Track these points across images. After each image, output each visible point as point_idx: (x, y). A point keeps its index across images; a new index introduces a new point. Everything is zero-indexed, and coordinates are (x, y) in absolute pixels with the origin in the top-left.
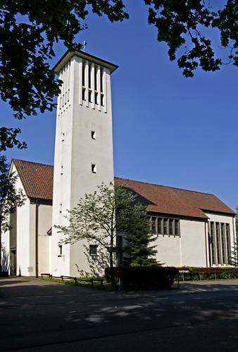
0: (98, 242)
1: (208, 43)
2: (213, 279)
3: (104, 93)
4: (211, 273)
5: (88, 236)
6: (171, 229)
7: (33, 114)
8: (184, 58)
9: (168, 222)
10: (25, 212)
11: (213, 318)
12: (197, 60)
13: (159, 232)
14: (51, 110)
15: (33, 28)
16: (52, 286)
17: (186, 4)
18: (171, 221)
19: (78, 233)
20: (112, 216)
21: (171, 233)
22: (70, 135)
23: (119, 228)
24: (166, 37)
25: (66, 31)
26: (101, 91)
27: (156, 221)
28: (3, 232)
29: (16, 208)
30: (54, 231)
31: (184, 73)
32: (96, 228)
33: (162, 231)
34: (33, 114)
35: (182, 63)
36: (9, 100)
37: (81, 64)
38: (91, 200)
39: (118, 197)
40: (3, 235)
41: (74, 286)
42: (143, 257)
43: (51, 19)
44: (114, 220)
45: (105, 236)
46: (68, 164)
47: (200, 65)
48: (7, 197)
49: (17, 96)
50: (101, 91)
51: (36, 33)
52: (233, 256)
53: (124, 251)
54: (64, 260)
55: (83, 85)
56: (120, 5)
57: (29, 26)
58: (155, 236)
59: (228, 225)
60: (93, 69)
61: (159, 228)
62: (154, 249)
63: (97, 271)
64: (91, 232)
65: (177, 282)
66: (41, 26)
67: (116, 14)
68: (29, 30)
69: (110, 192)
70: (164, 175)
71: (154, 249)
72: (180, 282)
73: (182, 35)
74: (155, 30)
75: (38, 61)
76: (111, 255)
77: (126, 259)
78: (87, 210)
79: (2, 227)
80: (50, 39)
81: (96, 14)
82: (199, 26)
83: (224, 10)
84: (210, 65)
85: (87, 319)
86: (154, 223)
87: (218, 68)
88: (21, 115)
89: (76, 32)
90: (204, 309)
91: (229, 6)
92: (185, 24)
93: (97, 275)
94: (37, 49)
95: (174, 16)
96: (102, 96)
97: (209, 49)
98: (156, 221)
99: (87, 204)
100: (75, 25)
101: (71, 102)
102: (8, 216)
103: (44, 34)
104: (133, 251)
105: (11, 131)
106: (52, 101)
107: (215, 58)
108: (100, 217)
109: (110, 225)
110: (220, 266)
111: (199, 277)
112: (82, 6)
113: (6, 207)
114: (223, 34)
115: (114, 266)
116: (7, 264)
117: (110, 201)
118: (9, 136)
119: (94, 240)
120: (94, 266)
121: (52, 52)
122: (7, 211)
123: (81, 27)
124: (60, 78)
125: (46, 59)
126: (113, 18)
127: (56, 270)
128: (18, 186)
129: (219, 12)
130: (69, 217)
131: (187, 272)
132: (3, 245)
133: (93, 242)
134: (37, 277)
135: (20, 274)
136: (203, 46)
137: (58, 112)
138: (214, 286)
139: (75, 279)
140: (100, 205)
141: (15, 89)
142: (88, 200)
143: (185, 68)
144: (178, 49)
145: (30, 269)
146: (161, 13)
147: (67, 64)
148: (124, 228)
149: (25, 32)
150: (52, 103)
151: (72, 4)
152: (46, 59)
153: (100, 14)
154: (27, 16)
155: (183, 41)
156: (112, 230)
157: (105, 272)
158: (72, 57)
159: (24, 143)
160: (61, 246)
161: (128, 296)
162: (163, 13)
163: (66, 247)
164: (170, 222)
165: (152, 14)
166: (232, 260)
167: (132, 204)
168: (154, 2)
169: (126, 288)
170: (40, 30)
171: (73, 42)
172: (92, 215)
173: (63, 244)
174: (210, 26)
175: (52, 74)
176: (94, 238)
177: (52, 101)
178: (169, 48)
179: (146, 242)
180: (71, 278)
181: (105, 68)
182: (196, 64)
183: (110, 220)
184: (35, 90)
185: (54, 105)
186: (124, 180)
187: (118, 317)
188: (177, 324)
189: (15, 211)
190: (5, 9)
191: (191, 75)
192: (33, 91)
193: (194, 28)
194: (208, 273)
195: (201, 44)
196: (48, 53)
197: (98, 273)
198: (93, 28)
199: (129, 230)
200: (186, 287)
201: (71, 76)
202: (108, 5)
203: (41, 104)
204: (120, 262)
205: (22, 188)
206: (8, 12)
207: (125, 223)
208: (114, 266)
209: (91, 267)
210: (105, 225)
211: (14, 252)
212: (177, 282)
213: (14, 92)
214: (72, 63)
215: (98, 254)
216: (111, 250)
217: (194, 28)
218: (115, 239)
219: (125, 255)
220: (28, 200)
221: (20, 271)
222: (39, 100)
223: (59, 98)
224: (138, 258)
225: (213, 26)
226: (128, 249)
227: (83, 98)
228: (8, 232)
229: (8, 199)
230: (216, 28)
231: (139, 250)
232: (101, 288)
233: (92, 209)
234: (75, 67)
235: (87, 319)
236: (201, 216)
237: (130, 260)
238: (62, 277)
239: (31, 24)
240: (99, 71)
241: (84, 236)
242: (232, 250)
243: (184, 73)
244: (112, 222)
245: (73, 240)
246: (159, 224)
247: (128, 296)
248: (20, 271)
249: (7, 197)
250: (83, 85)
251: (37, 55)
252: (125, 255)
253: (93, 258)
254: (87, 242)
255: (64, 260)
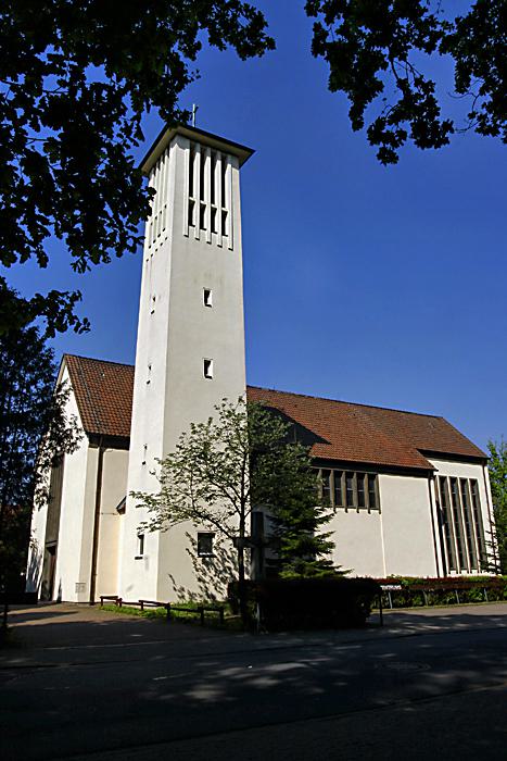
0: (214, 527)
1: (428, 87)
2: (453, 602)
3: (227, 208)
4: (448, 591)
5: (196, 514)
6: (361, 496)
7: (104, 261)
8: (380, 123)
9: (354, 481)
10: (79, 462)
11: (458, 687)
12: (406, 125)
13: (338, 503)
14: (133, 250)
15: (110, 89)
16: (120, 623)
17: (391, 8)
18: (360, 477)
19: (176, 509)
20: (243, 469)
21: (361, 505)
22: (166, 301)
23: (257, 495)
24: (346, 82)
25: (163, 89)
26: (223, 205)
27: (331, 477)
28: (36, 506)
29: (63, 455)
30: (131, 503)
31: (379, 156)
32: (210, 498)
33: (344, 501)
34: (104, 261)
35: (376, 135)
36: (66, 235)
37: (188, 151)
38: (203, 437)
39: (255, 429)
40: (35, 513)
41: (164, 624)
42: (307, 557)
43: (139, 68)
44: (246, 478)
45: (229, 514)
46: (160, 363)
47: (411, 137)
48: (49, 434)
49: (79, 226)
50: (223, 205)
51: (115, 98)
52: (489, 550)
53: (267, 545)
54: (147, 565)
55: (191, 194)
56: (258, 22)
57: (105, 87)
58: (329, 511)
59: (474, 482)
60: (208, 160)
61: (338, 494)
62: (327, 540)
63: (212, 590)
64: (202, 504)
65: (378, 611)
66: (123, 83)
67: (252, 42)
68: (104, 93)
69: (239, 418)
70: (349, 381)
71: (327, 540)
72: (385, 612)
73: (379, 75)
74: (323, 67)
75: (116, 153)
76: (241, 555)
77: (270, 561)
78: (195, 459)
79: (35, 497)
80: (137, 107)
81: (216, 47)
82: (414, 53)
83: (469, 17)
84: (431, 134)
85: (190, 694)
86: (327, 483)
87: (446, 141)
88: (85, 264)
89: (180, 88)
90: (438, 665)
91: (481, 8)
92: (386, 51)
93: (213, 597)
94: (116, 128)
95: (363, 35)
96: (224, 214)
97: (431, 101)
98: (331, 477)
99: (195, 445)
100: (179, 70)
101: (169, 231)
102: (47, 475)
103: (127, 100)
104: (286, 544)
105: (65, 298)
106: (136, 231)
107: (440, 119)
108: (217, 472)
109: (238, 489)
110: (464, 573)
111: (423, 601)
112: (192, 32)
113: (46, 455)
114: (460, 67)
115: (246, 577)
116: (36, 577)
117: (239, 437)
118: (62, 307)
119: (208, 522)
120: (207, 579)
121: (140, 134)
122: (47, 463)
123: (189, 76)
124: (150, 185)
125: (129, 147)
126: (245, 52)
127: (130, 588)
128: (71, 409)
129: (457, 20)
130: (159, 474)
131: (398, 587)
132: (34, 536)
133: (204, 526)
134: (92, 603)
135: (60, 598)
136: (418, 96)
137: (147, 253)
138: (455, 619)
139: (167, 606)
140: (219, 447)
141: (77, 212)
142: (196, 437)
143: (382, 145)
144: (368, 105)
145: (80, 586)
146: (338, 32)
147: (163, 154)
148: (265, 495)
149: (99, 97)
150: (137, 235)
151: (175, 33)
152: (129, 147)
153: (222, 47)
154: (103, 66)
155: (379, 86)
156: (243, 501)
157: (228, 589)
158: (172, 139)
159: (86, 320)
160: (141, 537)
161: (276, 643)
162: (342, 31)
163: (153, 538)
164: (357, 482)
165: (320, 33)
166: (490, 560)
167: (282, 442)
168: (325, 9)
169: (272, 625)
170: (122, 92)
171: (175, 109)
172: (203, 467)
173: (146, 532)
174: (435, 52)
175: (137, 181)
176: (207, 517)
177: (136, 231)
178: (351, 104)
179: (311, 524)
180: (159, 604)
181: (229, 158)
182: (403, 135)
183: (240, 479)
184: (107, 210)
185: (140, 241)
186: (265, 391)
187: (255, 690)
188: (383, 702)
189: (62, 462)
190: (72, 59)
191: (393, 158)
192: (105, 214)
193: (403, 58)
194: (442, 589)
195: (415, 90)
196: (132, 137)
197: (214, 593)
198: (211, 76)
199: (277, 499)
200: (398, 620)
201: (172, 177)
202: (237, 26)
203: (118, 240)
204: (258, 571)
205: (77, 414)
206: (76, 64)
207: (267, 486)
208: (246, 577)
209: (200, 580)
210: (230, 490)
211: (52, 550)
212: (378, 611)
213: (75, 220)
214: (172, 150)
215: (215, 552)
216: (240, 543)
217: (403, 58)
218: (248, 520)
219: (269, 554)
220: (86, 440)
221: (60, 591)
222: (115, 232)
223: (148, 224)
224: (296, 560)
225: (442, 51)
226: (276, 542)
227: (190, 223)
228: (45, 507)
229: (51, 439)
230: (449, 54)
231: (297, 543)
232: (220, 625)
233: (204, 455)
234: (178, 155)
235: (190, 694)
236: (419, 466)
237: (279, 565)
238: (141, 603)
239: (107, 81)
240: (219, 163)
241: (187, 515)
242: (488, 537)
243: (379, 156)
244: (242, 482)
245: (167, 522)
246: (337, 484)
247: (276, 643)
248: (60, 591)
249: (49, 434)
250: (191, 194)
251: (116, 141)
252: (269, 554)
253: (204, 562)
254: (193, 528)
255: (147, 565)
